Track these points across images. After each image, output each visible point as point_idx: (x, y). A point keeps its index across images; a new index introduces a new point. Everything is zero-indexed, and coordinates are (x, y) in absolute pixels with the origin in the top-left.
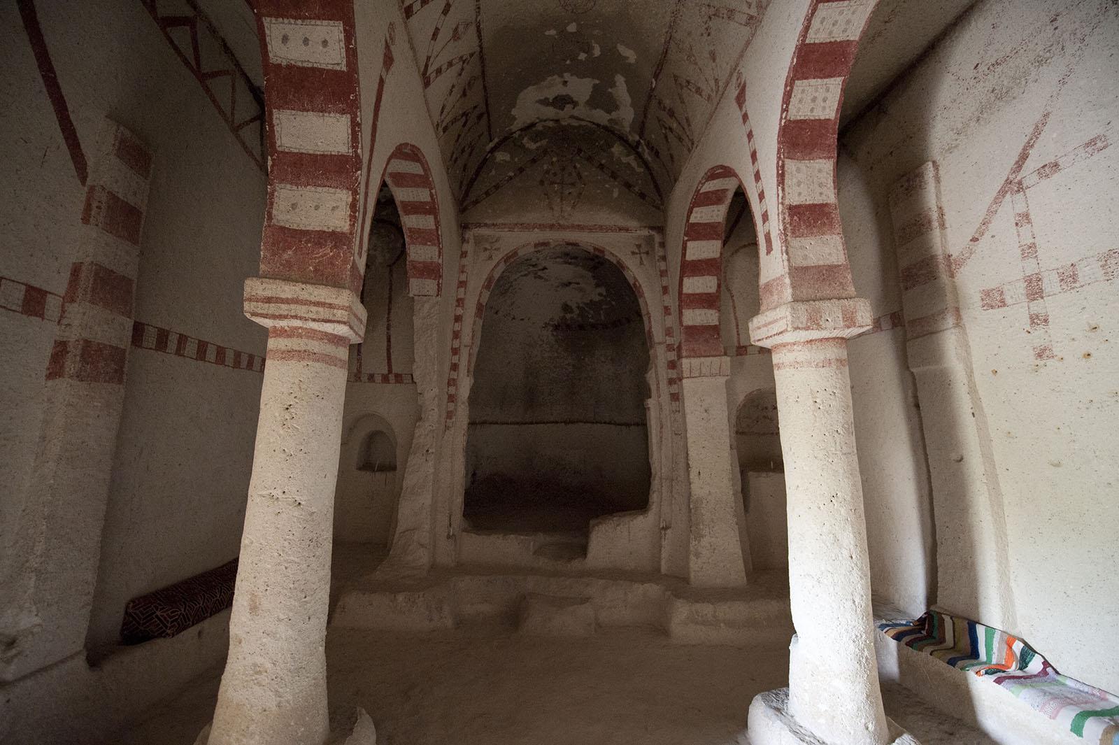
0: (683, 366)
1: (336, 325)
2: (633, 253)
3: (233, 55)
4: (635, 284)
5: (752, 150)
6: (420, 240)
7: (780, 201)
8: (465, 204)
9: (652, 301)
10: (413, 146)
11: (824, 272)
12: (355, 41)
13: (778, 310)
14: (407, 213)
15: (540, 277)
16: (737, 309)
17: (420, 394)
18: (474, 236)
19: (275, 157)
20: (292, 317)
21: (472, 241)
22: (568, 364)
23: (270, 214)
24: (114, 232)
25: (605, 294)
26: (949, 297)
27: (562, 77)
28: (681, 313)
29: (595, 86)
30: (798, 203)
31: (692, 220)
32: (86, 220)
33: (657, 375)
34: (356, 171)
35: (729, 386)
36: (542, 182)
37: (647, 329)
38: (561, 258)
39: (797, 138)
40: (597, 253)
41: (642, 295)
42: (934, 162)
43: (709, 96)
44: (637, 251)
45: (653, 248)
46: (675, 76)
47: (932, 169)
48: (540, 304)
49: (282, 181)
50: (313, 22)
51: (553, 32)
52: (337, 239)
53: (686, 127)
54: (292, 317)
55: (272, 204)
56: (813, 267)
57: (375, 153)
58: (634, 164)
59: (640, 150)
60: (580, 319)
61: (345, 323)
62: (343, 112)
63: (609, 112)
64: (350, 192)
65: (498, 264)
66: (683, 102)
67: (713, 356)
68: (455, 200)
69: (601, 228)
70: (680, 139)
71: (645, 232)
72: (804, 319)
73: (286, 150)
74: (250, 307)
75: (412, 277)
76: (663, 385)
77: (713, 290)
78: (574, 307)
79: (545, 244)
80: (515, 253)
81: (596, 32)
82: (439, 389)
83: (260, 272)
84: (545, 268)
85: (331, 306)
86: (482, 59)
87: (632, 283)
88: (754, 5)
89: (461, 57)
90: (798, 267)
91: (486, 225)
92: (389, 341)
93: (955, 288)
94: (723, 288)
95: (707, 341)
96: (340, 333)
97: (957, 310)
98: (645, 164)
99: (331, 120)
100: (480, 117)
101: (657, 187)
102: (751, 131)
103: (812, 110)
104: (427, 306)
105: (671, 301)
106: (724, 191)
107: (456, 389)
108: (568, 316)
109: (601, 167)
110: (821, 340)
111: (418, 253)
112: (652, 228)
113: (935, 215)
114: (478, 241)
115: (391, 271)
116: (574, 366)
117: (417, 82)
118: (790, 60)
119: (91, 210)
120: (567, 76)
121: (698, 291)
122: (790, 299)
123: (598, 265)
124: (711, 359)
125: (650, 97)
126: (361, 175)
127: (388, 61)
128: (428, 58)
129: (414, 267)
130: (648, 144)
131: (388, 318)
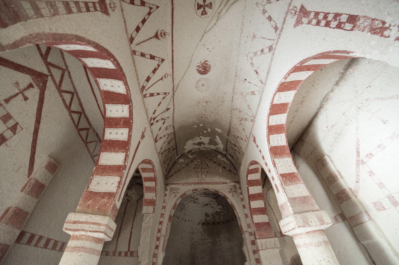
0: (258, 244)
1: (99, 233)
2: (230, 192)
3: (99, 136)
4: (232, 205)
5: (262, 156)
6: (149, 191)
7: (276, 173)
8: (167, 177)
9: (240, 212)
10: (149, 160)
11: (303, 199)
12: (131, 133)
13: (289, 217)
14: (146, 181)
15: (196, 202)
16: (275, 214)
17: (140, 263)
18: (170, 188)
19: (97, 167)
20: (82, 230)
21: (169, 190)
22: (210, 242)
23: (88, 186)
24: (31, 194)
25: (221, 208)
26: (360, 207)
27: (200, 137)
28: (252, 217)
29: (210, 139)
30: (283, 173)
31: (249, 179)
32: (22, 191)
33: (247, 248)
34: (124, 170)
35: (282, 253)
36: (194, 168)
37: (240, 225)
38: (203, 194)
39: (276, 152)
40: (216, 193)
41: (235, 209)
42: (327, 155)
43: (245, 140)
44: (231, 191)
45: (237, 189)
46: (234, 135)
47: (328, 158)
48: (196, 214)
49: (97, 174)
50: (120, 129)
51: (196, 126)
52: (110, 195)
53: (240, 149)
54: (82, 230)
55: (90, 183)
56: (297, 197)
57: (133, 163)
58: (225, 161)
59: (227, 156)
60: (213, 220)
61: (103, 232)
62: (123, 152)
63: (215, 146)
64: (120, 178)
65: (178, 198)
66: (238, 142)
67: (270, 238)
68: (164, 175)
69: (216, 183)
70: (239, 153)
71: (233, 184)
72: (301, 221)
73: (102, 165)
74: (66, 226)
75: (144, 206)
76: (251, 254)
77: (263, 206)
78: (210, 214)
79: (196, 190)
80: (185, 194)
81: (208, 126)
82: (148, 260)
83: (76, 210)
84: (197, 199)
85: (99, 224)
86: (175, 134)
87: (230, 204)
88: (252, 117)
89: (168, 134)
90: (292, 198)
91: (174, 183)
92: (131, 234)
93: (360, 202)
94: (267, 205)
95: (266, 230)
96: (101, 237)
97: (366, 212)
98: (230, 160)
99: (119, 154)
100: (174, 149)
101: (234, 167)
102: (260, 150)
103: (278, 143)
104: (148, 218)
105: (247, 211)
106: (258, 168)
107: (156, 260)
108: (208, 219)
109: (215, 162)
110: (313, 232)
111: (148, 196)
112: (235, 182)
113: (337, 174)
114: (171, 190)
115: (137, 203)
116: (212, 243)
117: (153, 142)
118: (266, 130)
119: (26, 187)
120: (201, 137)
121: (257, 207)
122: (292, 213)
123: (217, 197)
124: (269, 239)
125: (227, 141)
126: (125, 172)
127: (143, 136)
128: (157, 135)
129: (146, 201)
130: (229, 154)
131: (133, 223)
